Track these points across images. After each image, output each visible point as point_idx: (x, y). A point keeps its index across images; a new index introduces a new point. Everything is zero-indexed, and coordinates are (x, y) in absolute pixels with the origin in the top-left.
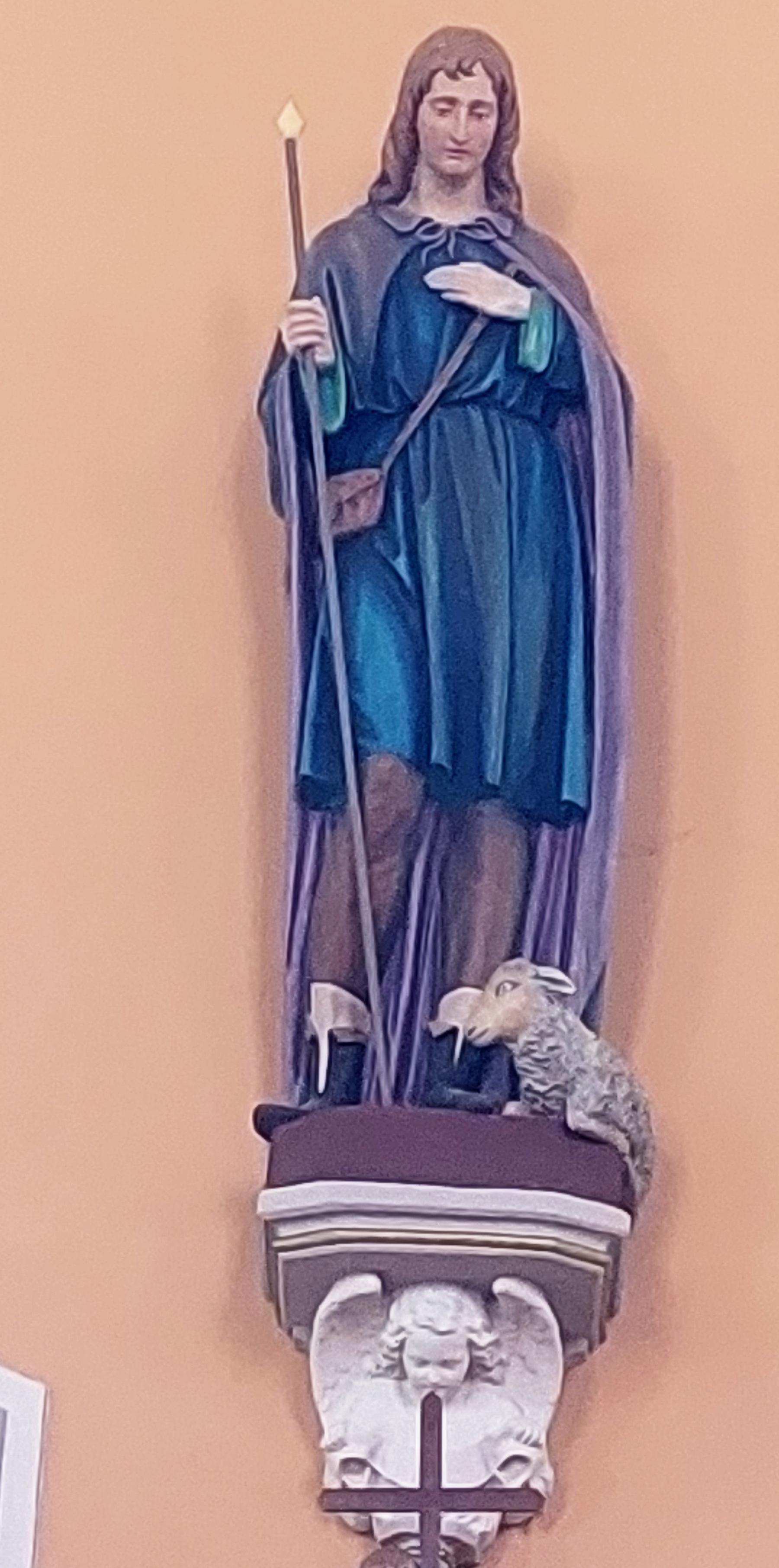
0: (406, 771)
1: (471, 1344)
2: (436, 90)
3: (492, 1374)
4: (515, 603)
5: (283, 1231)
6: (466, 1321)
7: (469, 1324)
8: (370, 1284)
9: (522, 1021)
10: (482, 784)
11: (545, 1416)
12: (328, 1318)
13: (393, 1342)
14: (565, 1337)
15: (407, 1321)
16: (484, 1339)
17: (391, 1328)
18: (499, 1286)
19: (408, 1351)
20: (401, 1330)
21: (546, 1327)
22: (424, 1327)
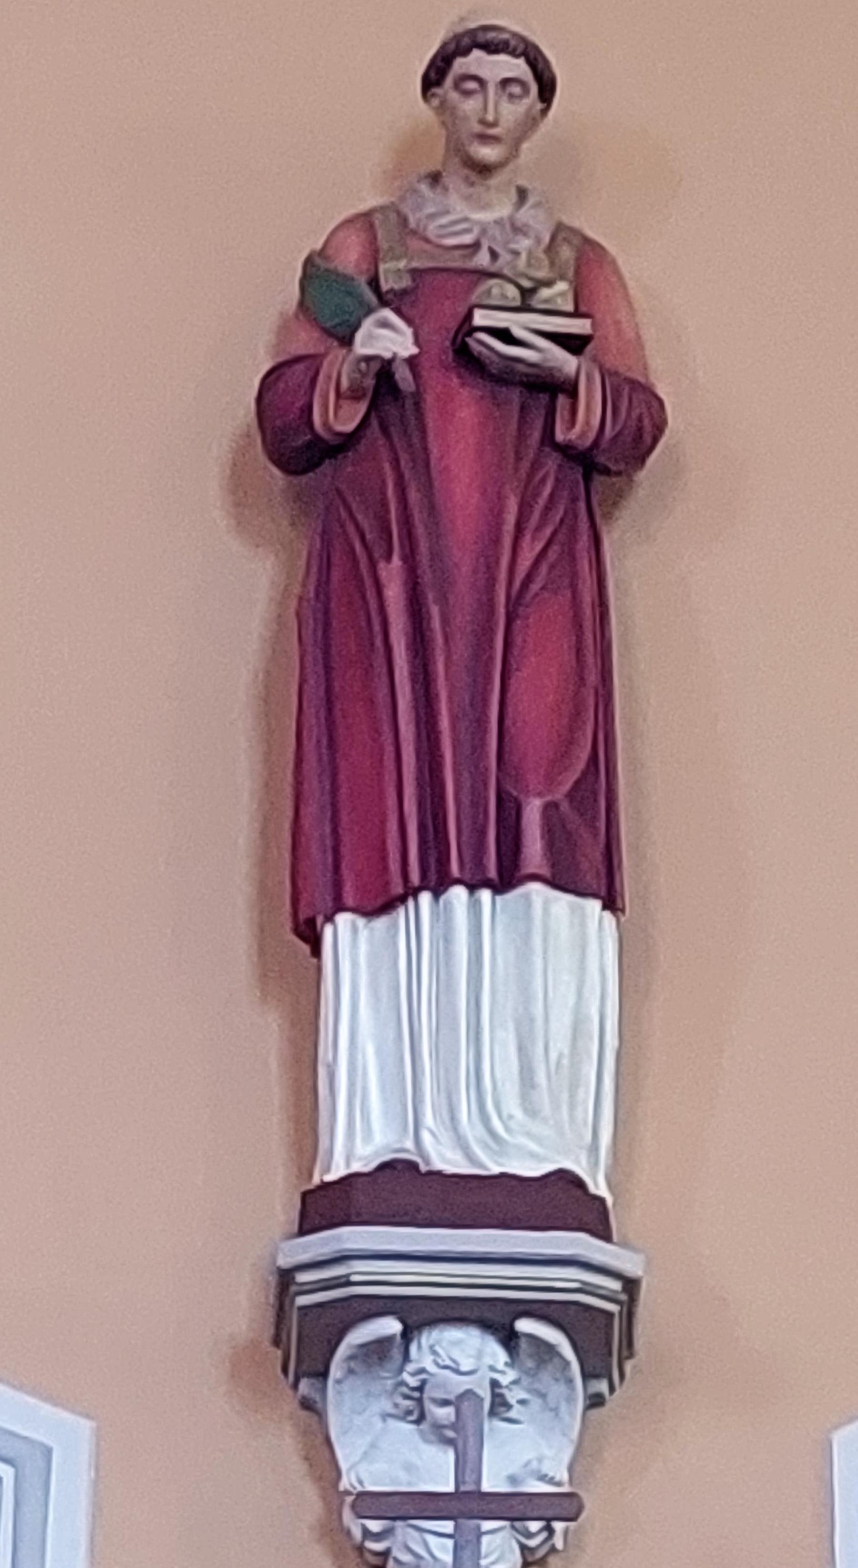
0: (519, 622)
1: (494, 1384)
2: (491, 1422)
3: (512, 1414)
4: (302, 806)
5: (303, 1277)
6: (488, 1361)
7: (491, 1362)
8: (391, 1326)
9: (421, 227)
10: (417, 287)
11: (566, 1456)
12: (351, 1358)
13: (413, 1382)
14: (586, 1376)
15: (428, 1363)
16: (504, 1380)
17: (411, 1367)
18: (524, 1325)
19: (428, 1393)
20: (422, 1371)
21: (567, 1364)
22: (446, 1367)
